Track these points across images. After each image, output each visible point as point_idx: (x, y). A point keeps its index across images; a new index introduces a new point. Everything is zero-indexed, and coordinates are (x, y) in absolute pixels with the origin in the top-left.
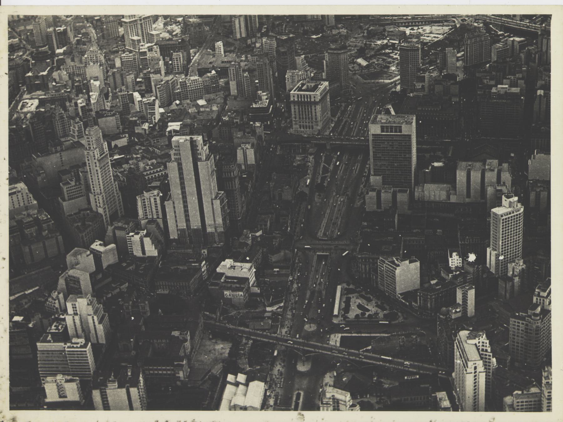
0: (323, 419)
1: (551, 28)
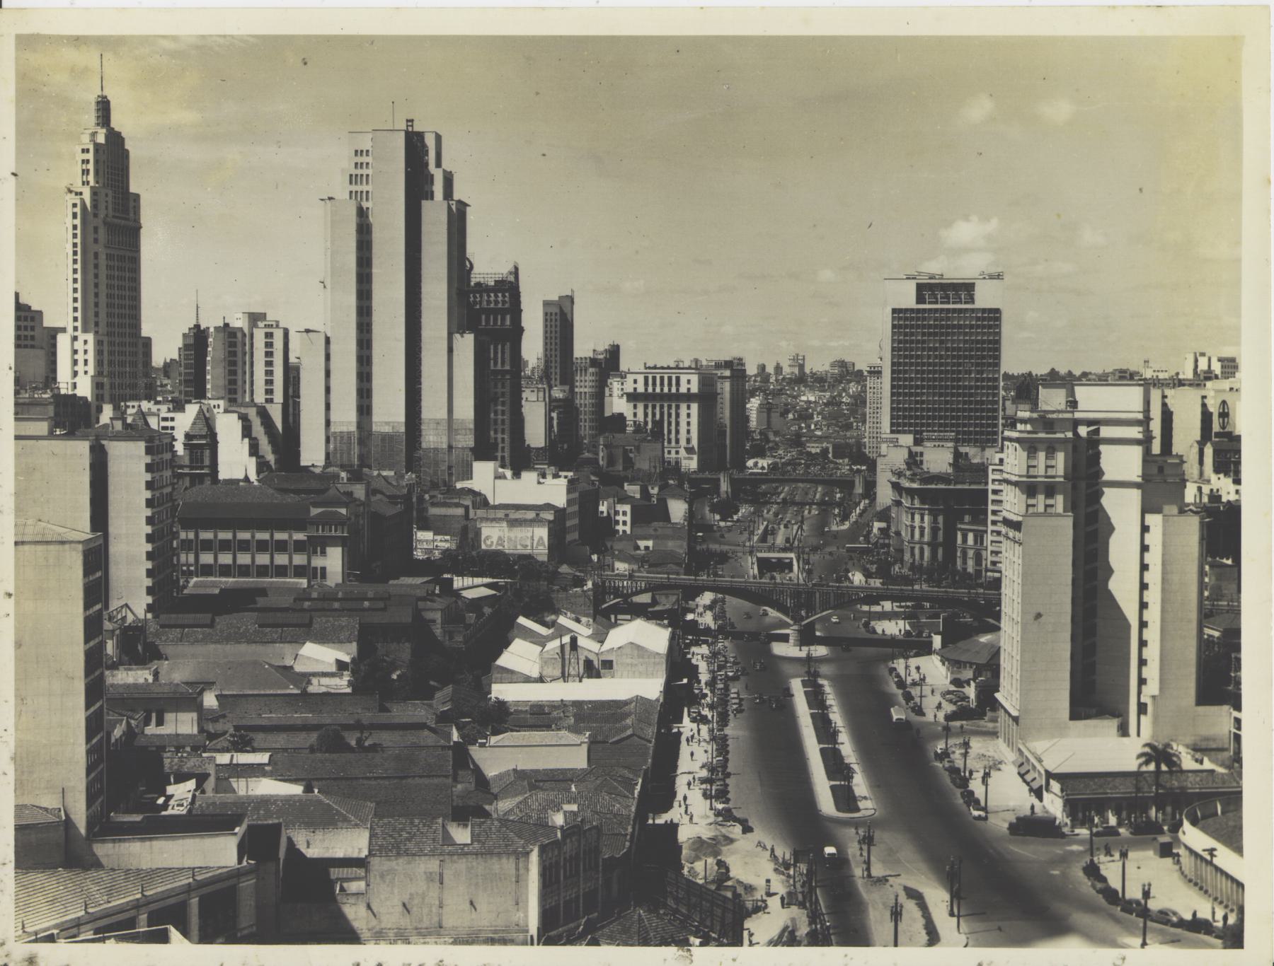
1: (584, 948)
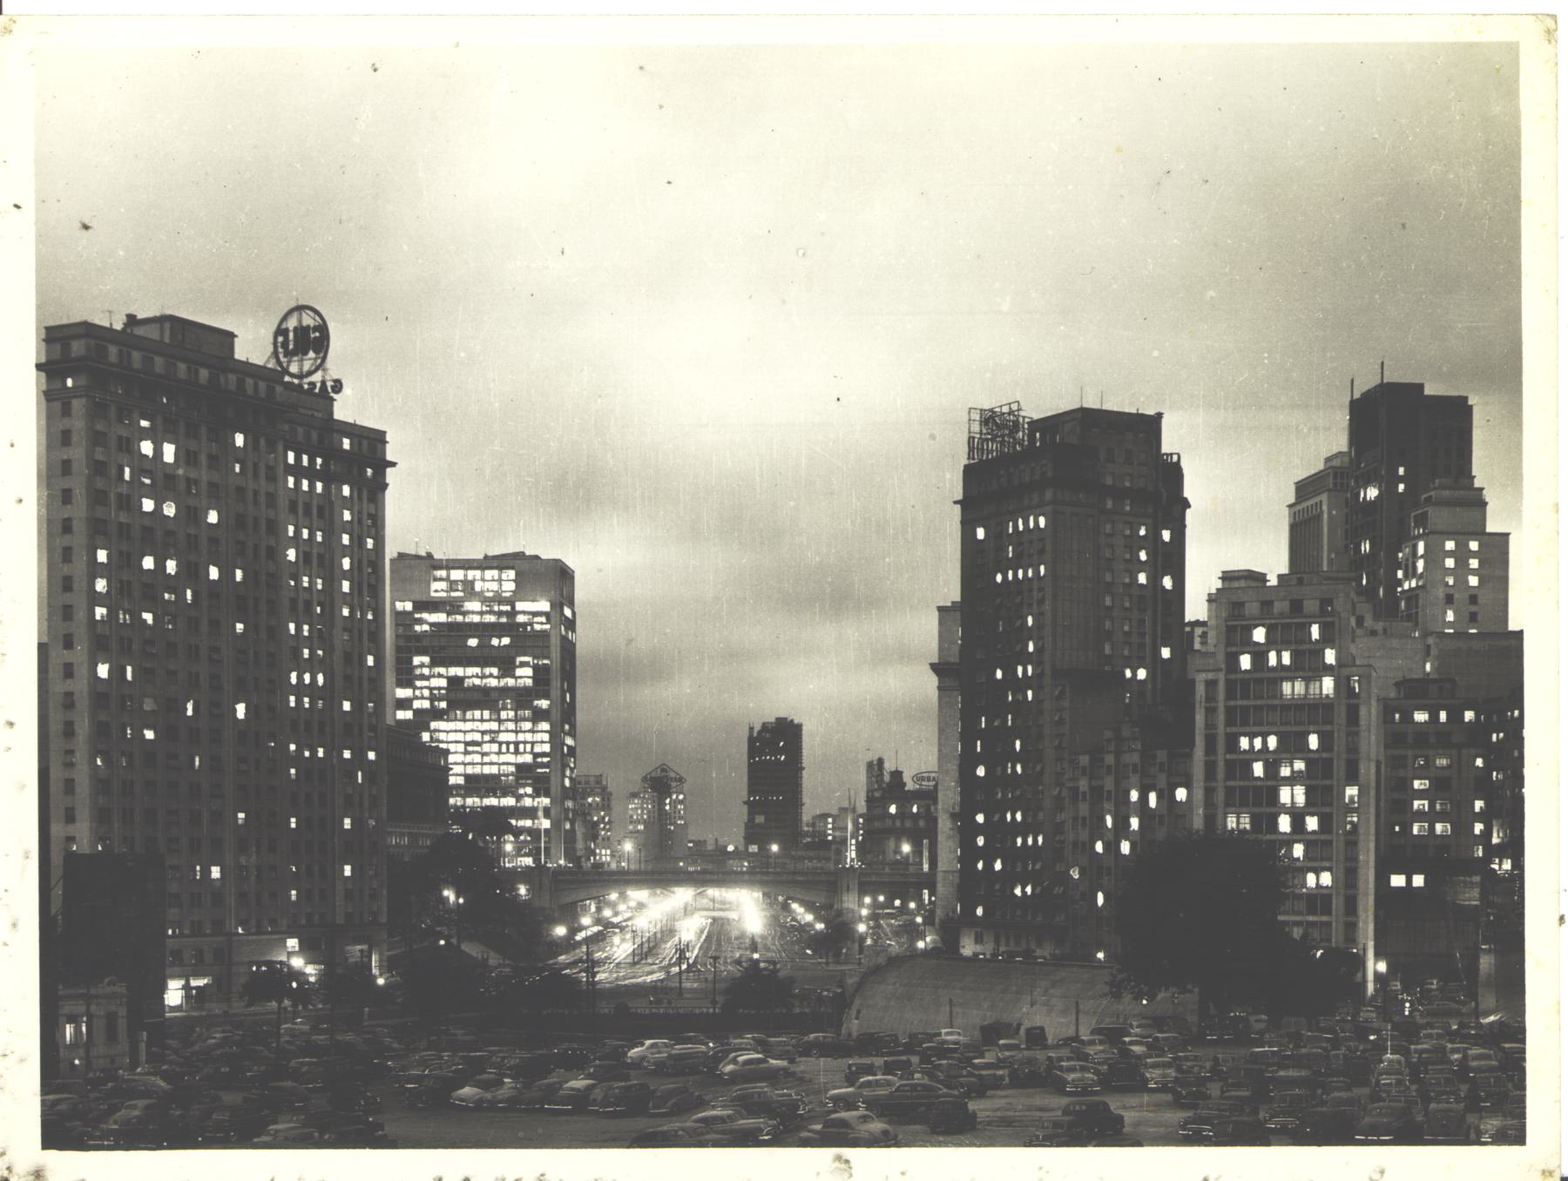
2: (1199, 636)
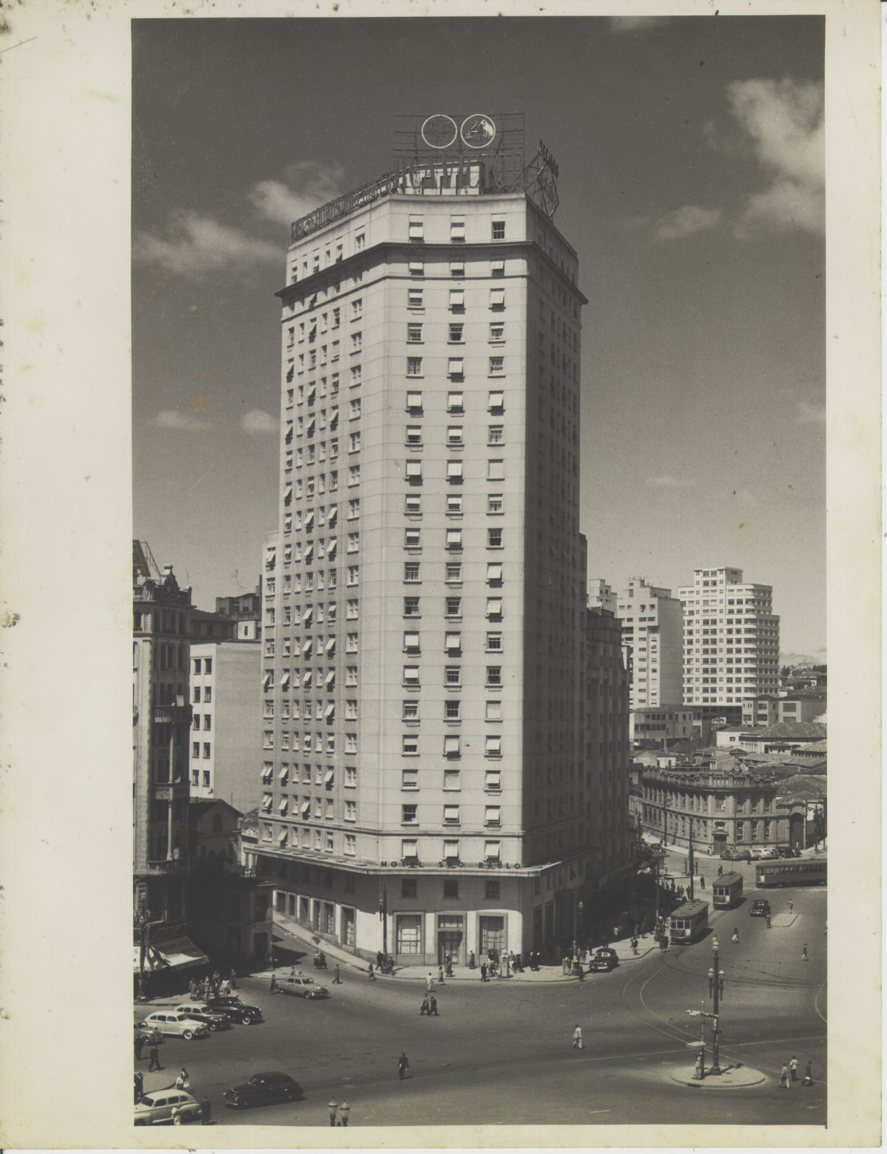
0: (6, 665)
2: (274, 980)
